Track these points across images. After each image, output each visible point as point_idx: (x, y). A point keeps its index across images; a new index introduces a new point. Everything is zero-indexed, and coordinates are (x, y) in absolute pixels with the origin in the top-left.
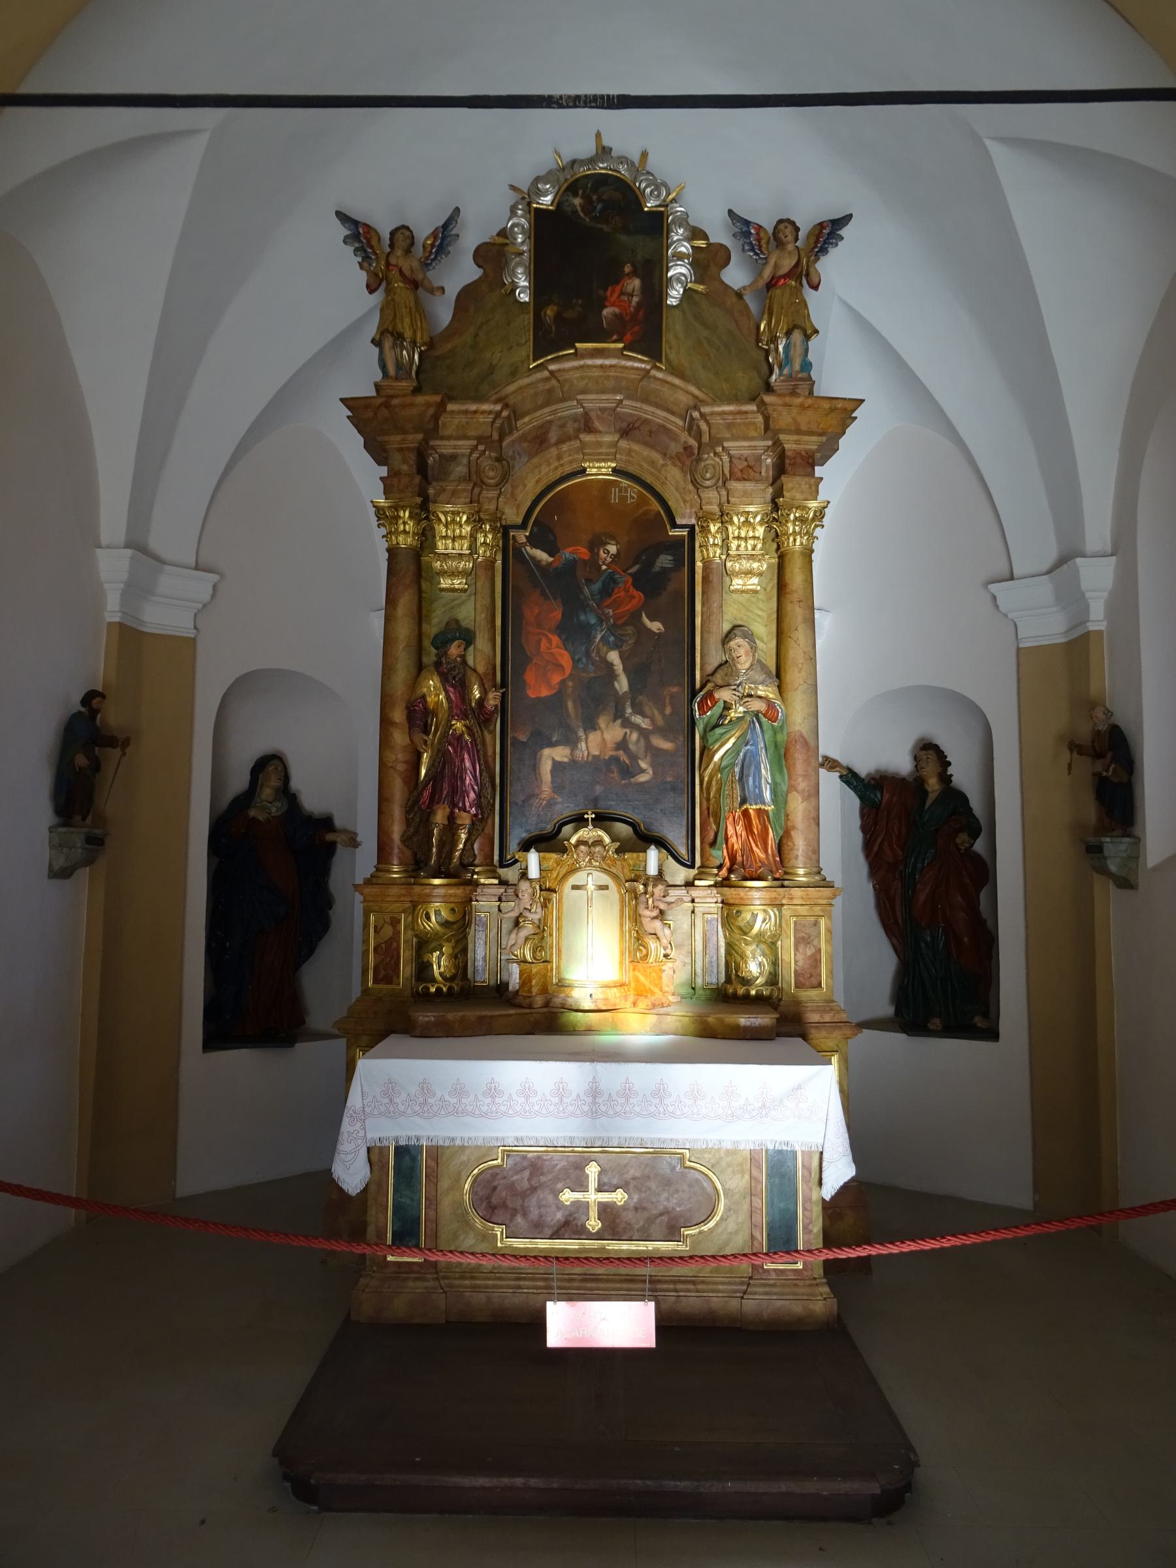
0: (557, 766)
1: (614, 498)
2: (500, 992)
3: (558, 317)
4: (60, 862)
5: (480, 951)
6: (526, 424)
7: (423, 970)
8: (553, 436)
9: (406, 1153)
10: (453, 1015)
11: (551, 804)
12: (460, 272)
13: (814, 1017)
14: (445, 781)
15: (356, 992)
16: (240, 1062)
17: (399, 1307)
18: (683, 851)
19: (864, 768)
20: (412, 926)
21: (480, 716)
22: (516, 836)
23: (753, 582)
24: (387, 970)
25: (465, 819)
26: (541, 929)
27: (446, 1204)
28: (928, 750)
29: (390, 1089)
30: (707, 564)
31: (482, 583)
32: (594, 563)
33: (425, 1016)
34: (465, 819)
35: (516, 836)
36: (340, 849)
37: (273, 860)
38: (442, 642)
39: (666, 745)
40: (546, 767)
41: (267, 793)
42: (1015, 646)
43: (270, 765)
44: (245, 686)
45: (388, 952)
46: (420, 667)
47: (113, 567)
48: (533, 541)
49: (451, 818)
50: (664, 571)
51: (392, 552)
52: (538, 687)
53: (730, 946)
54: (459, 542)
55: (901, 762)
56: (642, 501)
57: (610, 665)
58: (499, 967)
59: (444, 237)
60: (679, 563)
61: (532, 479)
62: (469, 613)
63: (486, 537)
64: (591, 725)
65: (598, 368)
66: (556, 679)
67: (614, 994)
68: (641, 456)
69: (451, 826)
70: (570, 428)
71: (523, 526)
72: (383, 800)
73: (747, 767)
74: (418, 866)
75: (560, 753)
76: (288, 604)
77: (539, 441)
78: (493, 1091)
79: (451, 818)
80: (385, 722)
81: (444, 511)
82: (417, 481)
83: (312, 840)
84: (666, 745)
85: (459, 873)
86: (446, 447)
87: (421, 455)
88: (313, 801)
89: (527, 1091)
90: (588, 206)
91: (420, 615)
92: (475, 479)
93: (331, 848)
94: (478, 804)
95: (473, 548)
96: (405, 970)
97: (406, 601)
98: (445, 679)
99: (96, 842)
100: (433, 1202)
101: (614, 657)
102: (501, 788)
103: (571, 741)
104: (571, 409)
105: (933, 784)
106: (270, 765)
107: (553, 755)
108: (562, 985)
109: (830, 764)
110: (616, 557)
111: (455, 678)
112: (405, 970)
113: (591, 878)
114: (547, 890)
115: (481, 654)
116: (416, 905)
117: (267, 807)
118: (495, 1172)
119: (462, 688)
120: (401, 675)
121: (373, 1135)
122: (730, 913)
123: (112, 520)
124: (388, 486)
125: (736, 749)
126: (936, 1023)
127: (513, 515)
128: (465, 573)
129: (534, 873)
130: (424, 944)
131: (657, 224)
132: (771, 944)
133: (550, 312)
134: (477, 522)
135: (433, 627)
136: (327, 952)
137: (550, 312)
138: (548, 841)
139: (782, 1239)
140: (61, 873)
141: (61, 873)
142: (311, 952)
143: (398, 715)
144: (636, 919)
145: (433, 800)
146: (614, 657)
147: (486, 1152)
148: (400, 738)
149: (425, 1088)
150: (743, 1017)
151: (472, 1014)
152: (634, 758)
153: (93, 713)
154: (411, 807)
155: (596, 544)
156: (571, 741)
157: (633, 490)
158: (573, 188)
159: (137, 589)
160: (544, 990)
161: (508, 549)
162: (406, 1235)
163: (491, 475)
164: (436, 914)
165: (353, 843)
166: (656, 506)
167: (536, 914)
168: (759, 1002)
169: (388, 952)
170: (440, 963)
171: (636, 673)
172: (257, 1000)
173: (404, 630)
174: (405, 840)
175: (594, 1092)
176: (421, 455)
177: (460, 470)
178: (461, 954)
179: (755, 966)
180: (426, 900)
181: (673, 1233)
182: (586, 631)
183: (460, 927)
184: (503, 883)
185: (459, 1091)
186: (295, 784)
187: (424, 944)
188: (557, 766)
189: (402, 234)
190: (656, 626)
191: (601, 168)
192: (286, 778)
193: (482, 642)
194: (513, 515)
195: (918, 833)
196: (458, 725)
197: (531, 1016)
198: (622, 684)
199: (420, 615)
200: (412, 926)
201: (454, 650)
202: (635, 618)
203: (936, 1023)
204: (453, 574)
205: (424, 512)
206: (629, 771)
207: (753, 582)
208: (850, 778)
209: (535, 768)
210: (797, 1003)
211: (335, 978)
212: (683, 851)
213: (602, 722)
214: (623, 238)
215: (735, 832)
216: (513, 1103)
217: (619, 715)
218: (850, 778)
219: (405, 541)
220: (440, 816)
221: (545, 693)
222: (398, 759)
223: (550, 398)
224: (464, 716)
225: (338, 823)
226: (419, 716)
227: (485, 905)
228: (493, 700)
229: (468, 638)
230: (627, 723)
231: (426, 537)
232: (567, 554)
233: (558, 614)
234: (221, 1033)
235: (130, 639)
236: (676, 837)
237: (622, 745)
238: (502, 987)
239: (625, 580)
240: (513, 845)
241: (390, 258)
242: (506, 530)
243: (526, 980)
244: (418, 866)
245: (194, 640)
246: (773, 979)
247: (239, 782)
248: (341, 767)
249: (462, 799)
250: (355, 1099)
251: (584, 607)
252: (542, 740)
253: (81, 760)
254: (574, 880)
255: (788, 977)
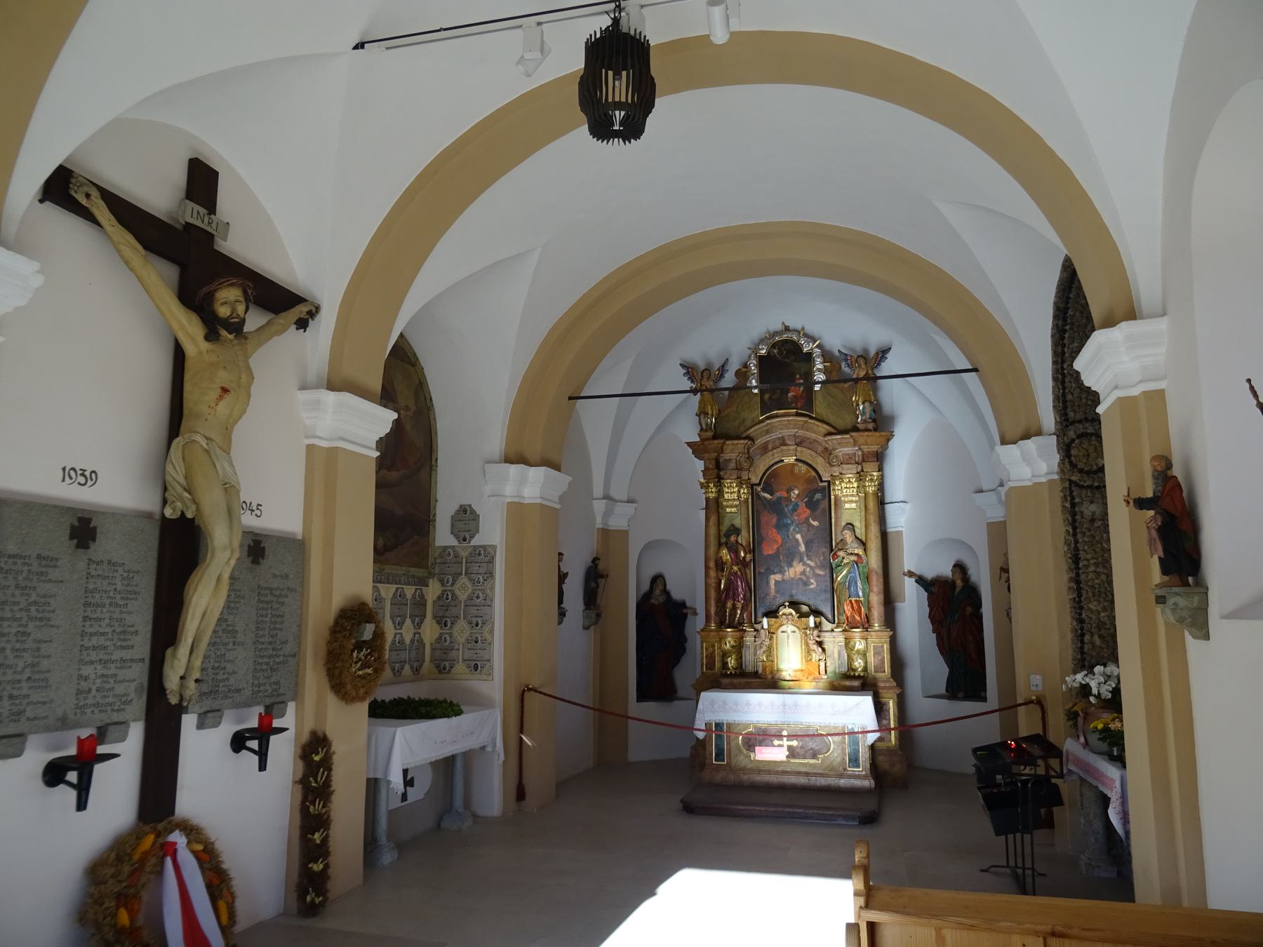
0: (777, 582)
1: (796, 471)
2: (755, 674)
3: (770, 398)
4: (587, 623)
5: (748, 657)
6: (759, 442)
7: (725, 665)
8: (770, 447)
9: (719, 726)
10: (735, 681)
11: (775, 598)
12: (729, 380)
13: (882, 684)
14: (731, 591)
15: (698, 674)
16: (651, 709)
17: (718, 777)
18: (830, 617)
19: (929, 574)
20: (720, 648)
21: (744, 564)
22: (761, 611)
23: (854, 505)
24: (711, 665)
25: (739, 605)
26: (770, 648)
27: (733, 744)
28: (960, 567)
29: (712, 703)
30: (836, 496)
31: (744, 508)
32: (788, 499)
33: (726, 681)
34: (739, 605)
35: (761, 611)
36: (690, 617)
37: (662, 620)
38: (728, 535)
39: (821, 573)
40: (772, 583)
41: (657, 592)
42: (1255, 402)
43: (658, 579)
44: (648, 547)
45: (711, 657)
46: (720, 545)
47: (599, 507)
48: (764, 490)
49: (734, 605)
50: (818, 501)
51: (707, 500)
52: (768, 550)
53: (848, 656)
54: (733, 493)
55: (946, 570)
56: (808, 472)
57: (797, 540)
58: (756, 662)
59: (723, 370)
60: (824, 497)
61: (762, 465)
62: (738, 522)
63: (744, 490)
64: (790, 565)
65: (786, 424)
66: (775, 547)
67: (799, 676)
68: (807, 454)
69: (734, 608)
70: (777, 443)
71: (759, 484)
72: (707, 598)
73: (853, 582)
74: (722, 624)
75: (778, 577)
76: (672, 535)
77: (765, 449)
78: (748, 704)
79: (734, 605)
80: (707, 567)
81: (727, 482)
82: (716, 473)
83: (676, 612)
84: (821, 573)
85: (738, 626)
86: (726, 456)
87: (717, 460)
88: (677, 595)
89: (760, 705)
90: (780, 352)
91: (719, 523)
92: (739, 468)
93: (686, 616)
94: (744, 599)
95: (739, 496)
96: (718, 665)
97: (713, 519)
98: (729, 550)
99: (598, 615)
100: (728, 743)
101: (798, 536)
102: (753, 592)
103: (782, 572)
104: (774, 436)
105: (959, 583)
106: (658, 579)
107: (774, 578)
108: (778, 670)
109: (911, 574)
110: (798, 496)
111: (734, 550)
112: (718, 665)
113: (789, 628)
114: (771, 633)
115: (743, 538)
116: (721, 639)
117: (658, 598)
118: (750, 734)
119: (737, 553)
120: (712, 549)
121: (707, 719)
122: (847, 641)
123: (598, 490)
124: (705, 472)
125: (846, 576)
126: (961, 695)
127: (755, 480)
128: (736, 506)
129: (766, 626)
130: (725, 655)
131: (809, 357)
132: (864, 654)
133: (767, 396)
134: (740, 485)
135: (724, 528)
136: (685, 661)
137: (767, 396)
138: (772, 614)
139: (854, 761)
140: (586, 628)
141: (586, 628)
142: (679, 661)
143: (712, 564)
144: (807, 644)
145: (727, 598)
146: (798, 536)
147: (747, 726)
148: (713, 573)
149: (725, 703)
150: (849, 682)
151: (743, 681)
152: (808, 578)
153: (596, 566)
154: (718, 600)
155: (789, 491)
156: (782, 572)
157: (804, 468)
158: (774, 346)
159: (608, 514)
160: (772, 672)
161: (754, 495)
162: (720, 756)
163: (746, 465)
164: (729, 643)
165: (695, 614)
166: (814, 473)
167: (767, 642)
168: (859, 677)
169: (711, 657)
170: (731, 662)
171: (807, 544)
172: (658, 682)
173: (713, 531)
174: (716, 614)
175: (784, 705)
176: (717, 460)
177: (733, 465)
178: (739, 658)
179: (858, 663)
180: (725, 637)
181: (814, 756)
182: (787, 526)
183: (739, 647)
184: (756, 630)
185: (736, 704)
186: (668, 587)
187: (725, 655)
188: (777, 582)
189: (707, 370)
190: (815, 523)
191: (785, 337)
192: (665, 585)
193: (744, 533)
194: (755, 480)
195: (953, 602)
196: (735, 568)
197: (769, 681)
198: (803, 548)
199: (719, 523)
200: (720, 648)
201: (733, 538)
202: (807, 519)
203: (961, 695)
204: (732, 507)
205: (719, 480)
206: (806, 584)
207: (854, 505)
208: (921, 580)
209: (768, 583)
210: (875, 679)
211: (686, 673)
212: (830, 617)
213: (795, 564)
214: (796, 364)
215: (847, 608)
216: (756, 708)
217: (801, 560)
218: (921, 580)
219: (712, 496)
220: (729, 604)
221: (771, 552)
222: (712, 581)
223: (768, 432)
224: (737, 564)
225: (688, 604)
226: (720, 565)
227: (749, 639)
228: (749, 557)
229: (737, 531)
230: (805, 564)
231: (720, 493)
232: (778, 494)
233: (774, 520)
234: (642, 697)
235: (605, 533)
236: (826, 610)
237: (803, 573)
238: (757, 672)
239: (802, 505)
240: (759, 614)
241: (702, 379)
242: (753, 485)
243: (764, 669)
244: (722, 624)
245: (627, 532)
246: (865, 669)
247: (646, 587)
248: (688, 580)
249: (741, 593)
250: (700, 706)
251: (786, 516)
252: (770, 571)
253: (593, 585)
254: (782, 628)
255: (871, 668)
